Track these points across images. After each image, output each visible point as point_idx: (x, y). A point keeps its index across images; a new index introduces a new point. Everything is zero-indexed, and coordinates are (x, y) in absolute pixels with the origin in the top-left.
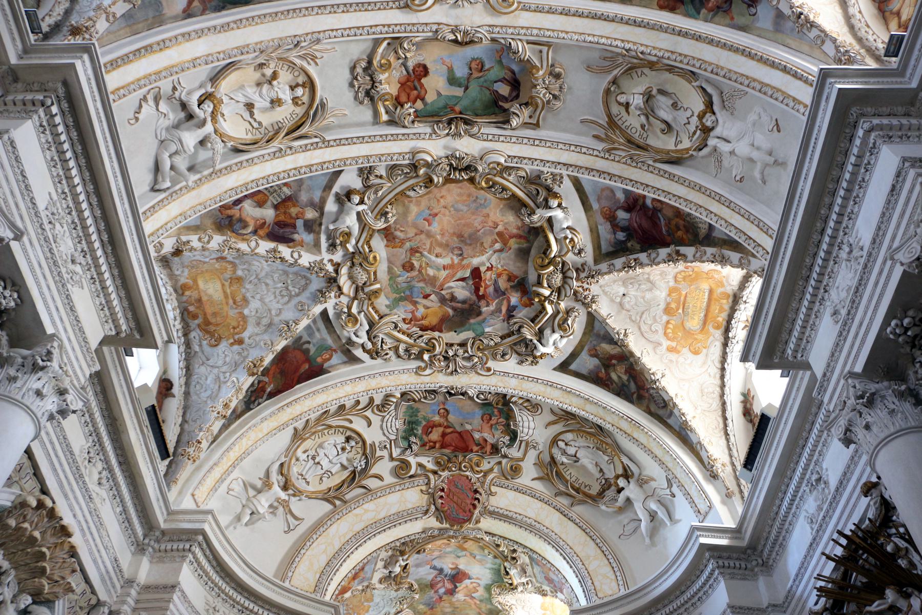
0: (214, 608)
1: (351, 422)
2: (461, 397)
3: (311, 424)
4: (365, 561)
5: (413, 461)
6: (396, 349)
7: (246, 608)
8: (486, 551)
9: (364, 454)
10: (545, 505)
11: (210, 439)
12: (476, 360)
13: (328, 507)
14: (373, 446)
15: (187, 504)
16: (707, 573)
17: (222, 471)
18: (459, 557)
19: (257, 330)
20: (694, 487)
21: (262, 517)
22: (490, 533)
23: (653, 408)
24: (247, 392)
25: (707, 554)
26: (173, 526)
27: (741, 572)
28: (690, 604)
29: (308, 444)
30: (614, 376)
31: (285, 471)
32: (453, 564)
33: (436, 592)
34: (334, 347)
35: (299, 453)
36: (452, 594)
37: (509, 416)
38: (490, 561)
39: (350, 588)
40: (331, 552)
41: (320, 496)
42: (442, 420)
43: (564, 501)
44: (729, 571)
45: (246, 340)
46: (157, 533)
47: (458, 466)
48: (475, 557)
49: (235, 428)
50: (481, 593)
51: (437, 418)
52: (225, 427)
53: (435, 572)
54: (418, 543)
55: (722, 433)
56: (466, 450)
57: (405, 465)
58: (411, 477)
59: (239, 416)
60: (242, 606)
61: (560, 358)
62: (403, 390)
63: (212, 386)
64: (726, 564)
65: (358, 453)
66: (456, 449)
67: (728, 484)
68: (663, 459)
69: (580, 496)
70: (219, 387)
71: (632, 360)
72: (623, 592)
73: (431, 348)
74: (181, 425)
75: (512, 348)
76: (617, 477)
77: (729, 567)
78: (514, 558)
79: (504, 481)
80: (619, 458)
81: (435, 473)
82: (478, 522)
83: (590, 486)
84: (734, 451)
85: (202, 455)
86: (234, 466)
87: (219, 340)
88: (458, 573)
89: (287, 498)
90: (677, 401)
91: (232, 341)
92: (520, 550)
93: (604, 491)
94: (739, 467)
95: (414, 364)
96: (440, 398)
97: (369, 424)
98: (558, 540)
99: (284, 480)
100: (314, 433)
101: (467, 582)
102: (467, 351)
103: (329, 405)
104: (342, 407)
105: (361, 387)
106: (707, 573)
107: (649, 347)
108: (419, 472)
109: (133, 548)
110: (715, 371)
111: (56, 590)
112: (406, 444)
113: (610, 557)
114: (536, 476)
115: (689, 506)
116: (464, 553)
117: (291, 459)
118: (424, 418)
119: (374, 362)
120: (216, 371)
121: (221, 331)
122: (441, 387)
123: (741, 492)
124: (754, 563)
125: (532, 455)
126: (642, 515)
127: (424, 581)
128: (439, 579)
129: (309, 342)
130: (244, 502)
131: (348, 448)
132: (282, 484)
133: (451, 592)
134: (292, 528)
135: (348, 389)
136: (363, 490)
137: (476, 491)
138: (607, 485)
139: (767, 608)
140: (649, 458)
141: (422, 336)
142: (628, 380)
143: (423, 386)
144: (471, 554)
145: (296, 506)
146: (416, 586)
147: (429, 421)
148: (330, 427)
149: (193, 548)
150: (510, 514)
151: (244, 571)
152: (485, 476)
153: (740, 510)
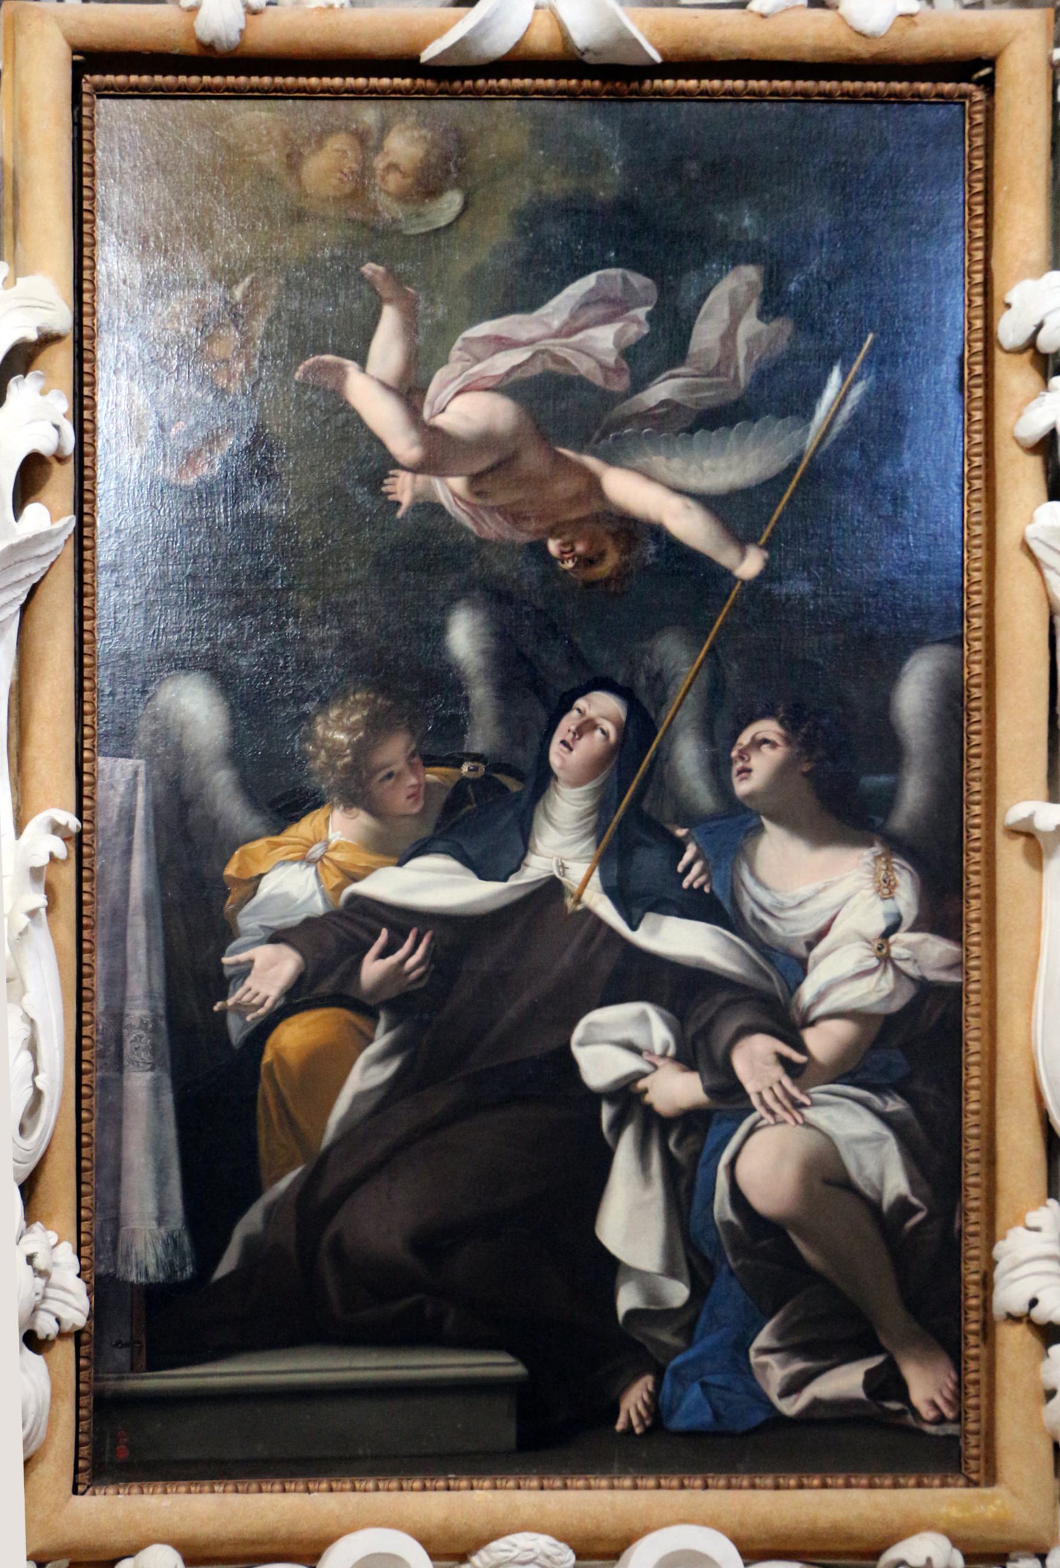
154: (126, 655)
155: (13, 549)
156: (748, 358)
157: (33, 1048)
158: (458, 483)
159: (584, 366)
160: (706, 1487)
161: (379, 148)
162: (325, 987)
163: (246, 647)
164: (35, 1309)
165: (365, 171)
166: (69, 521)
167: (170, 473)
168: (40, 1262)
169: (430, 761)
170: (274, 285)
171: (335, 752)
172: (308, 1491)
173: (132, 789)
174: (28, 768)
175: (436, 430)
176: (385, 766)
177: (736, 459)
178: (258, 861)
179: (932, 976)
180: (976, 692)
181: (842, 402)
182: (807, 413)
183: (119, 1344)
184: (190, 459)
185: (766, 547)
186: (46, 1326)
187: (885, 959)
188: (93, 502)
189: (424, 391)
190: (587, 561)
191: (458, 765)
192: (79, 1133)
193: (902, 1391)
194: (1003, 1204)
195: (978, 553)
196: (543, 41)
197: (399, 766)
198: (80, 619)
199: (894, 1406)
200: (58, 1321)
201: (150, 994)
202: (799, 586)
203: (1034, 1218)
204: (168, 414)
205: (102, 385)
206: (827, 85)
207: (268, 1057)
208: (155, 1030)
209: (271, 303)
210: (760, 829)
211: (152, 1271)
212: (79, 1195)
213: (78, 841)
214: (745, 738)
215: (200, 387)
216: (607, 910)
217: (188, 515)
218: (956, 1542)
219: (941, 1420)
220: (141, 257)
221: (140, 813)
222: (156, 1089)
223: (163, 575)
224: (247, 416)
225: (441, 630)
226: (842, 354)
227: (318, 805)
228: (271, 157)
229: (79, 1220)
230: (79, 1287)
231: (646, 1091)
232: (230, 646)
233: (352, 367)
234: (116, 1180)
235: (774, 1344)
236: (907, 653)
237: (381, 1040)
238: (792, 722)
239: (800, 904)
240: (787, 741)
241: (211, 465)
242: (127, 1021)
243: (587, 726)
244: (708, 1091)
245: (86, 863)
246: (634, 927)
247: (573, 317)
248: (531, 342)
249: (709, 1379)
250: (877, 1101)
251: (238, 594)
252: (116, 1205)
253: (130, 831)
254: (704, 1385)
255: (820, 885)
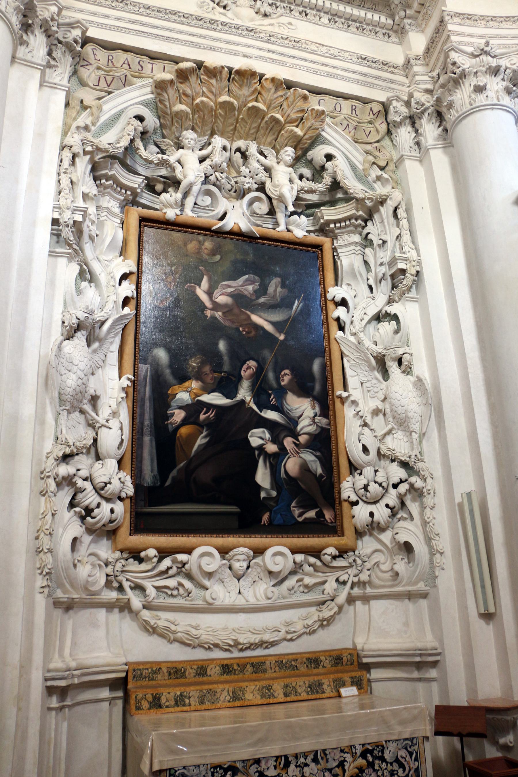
109: (394, 39)
111: (308, 124)
154: (146, 342)
155: (121, 316)
156: (279, 295)
157: (121, 429)
158: (220, 313)
159: (246, 293)
160: (282, 537)
161: (203, 245)
162: (192, 420)
163: (174, 343)
164: (121, 491)
165: (200, 248)
166: (134, 312)
167: (157, 304)
168: (122, 480)
169: (215, 372)
170: (181, 268)
171: (194, 368)
172: (188, 537)
173: (147, 371)
174: (123, 364)
175: (215, 302)
176: (205, 372)
177: (278, 315)
178: (176, 390)
179: (324, 426)
180: (328, 368)
181: (298, 306)
182: (292, 308)
183: (141, 500)
184: (162, 302)
185: (285, 334)
186: (123, 495)
187: (314, 422)
188: (140, 308)
189: (213, 294)
190: (248, 333)
191: (221, 373)
192: (132, 450)
193: (324, 516)
194: (341, 475)
195: (327, 339)
196: (236, 229)
197: (208, 372)
198: (136, 333)
199: (322, 519)
200: (126, 494)
201: (150, 419)
202: (292, 343)
203: (348, 479)
204: (157, 292)
205: (143, 284)
206: (291, 246)
207: (178, 435)
208: (151, 427)
209: (180, 272)
210: (287, 393)
211: (149, 483)
212: (132, 464)
213: (133, 382)
214: (283, 373)
215: (164, 287)
216: (255, 407)
217: (161, 313)
218: (337, 549)
219: (332, 522)
220: (152, 259)
221: (148, 377)
222: (151, 441)
223: (155, 326)
224: (175, 294)
225: (217, 344)
226: (298, 297)
227: (190, 379)
228: (181, 243)
229: (132, 470)
230: (131, 486)
231: (265, 448)
232: (170, 342)
233: (197, 287)
234: (141, 462)
235: (296, 505)
236: (314, 359)
237: (205, 433)
238: (292, 371)
239: (296, 409)
240: (291, 375)
241: (166, 303)
242: (144, 424)
243: (249, 368)
244: (278, 449)
245: (135, 387)
246: (261, 412)
247: (244, 283)
248: (235, 287)
249: (282, 513)
250: (314, 453)
251: (172, 331)
252: (141, 467)
253: (146, 381)
254: (281, 514)
255: (300, 405)
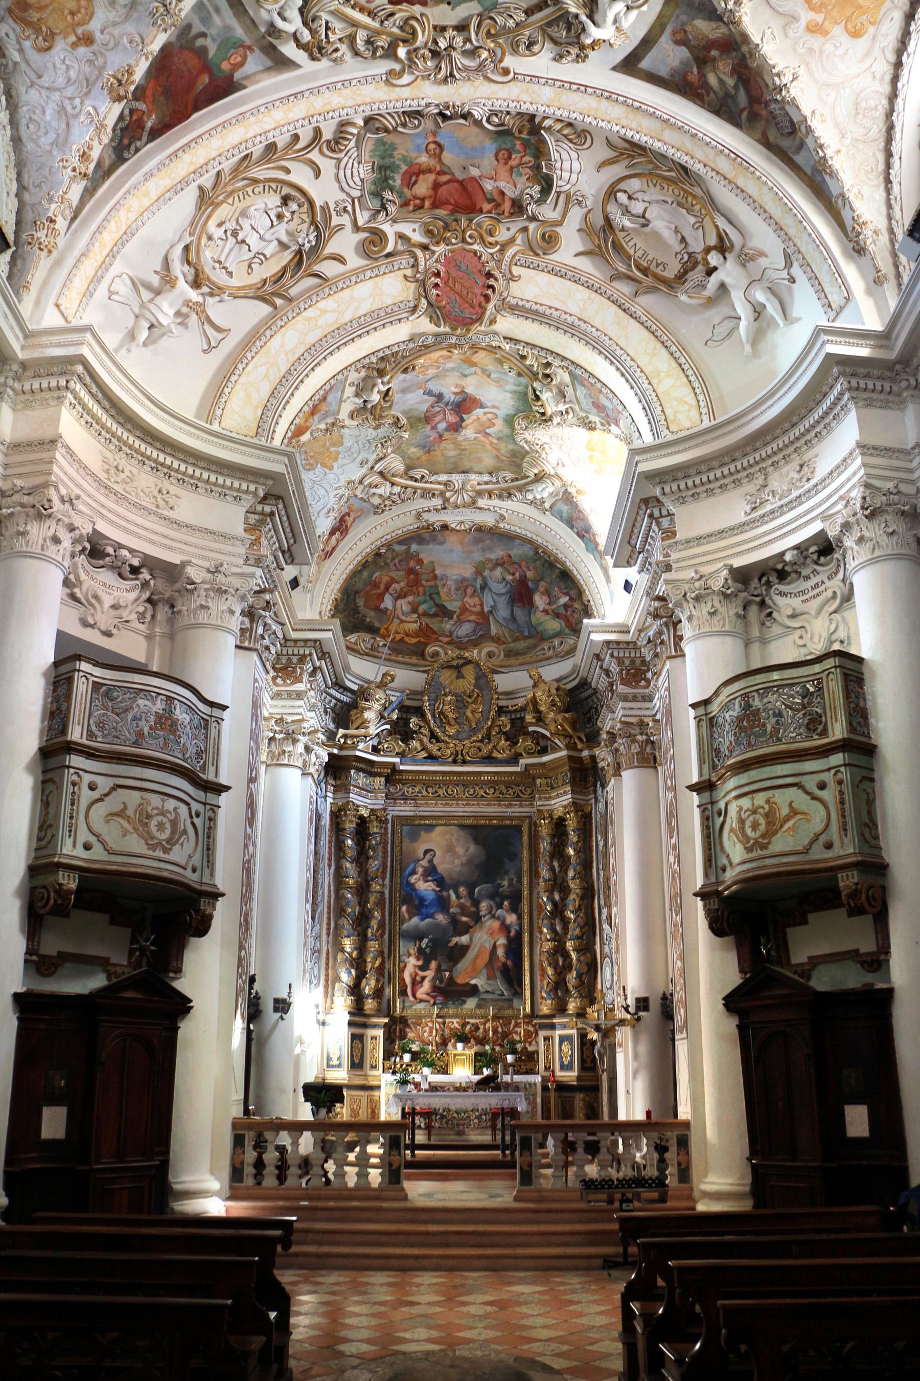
0: (116, 467)
1: (288, 171)
2: (462, 121)
3: (225, 178)
4: (328, 387)
5: (389, 230)
6: (352, 39)
7: (162, 465)
8: (506, 367)
9: (313, 222)
10: (594, 295)
11: (69, 214)
12: (485, 55)
13: (265, 309)
14: (325, 208)
15: (51, 319)
16: (832, 397)
17: (96, 265)
18: (466, 376)
19: (112, 16)
20: (826, 267)
21: (167, 332)
22: (511, 339)
23: (773, 136)
24: (114, 130)
25: (835, 370)
26: (36, 354)
27: (882, 397)
28: (802, 441)
29: (223, 212)
30: (712, 79)
31: (193, 257)
32: (457, 386)
33: (434, 428)
34: (248, 42)
35: (212, 226)
36: (456, 430)
37: (539, 151)
38: (511, 381)
39: (307, 428)
40: (275, 376)
41: (251, 293)
42: (432, 162)
43: (624, 288)
44: (866, 395)
45: (98, 35)
46: (15, 367)
47: (460, 236)
48: (489, 376)
49: (106, 193)
50: (499, 427)
51: (424, 159)
52: (88, 193)
53: (432, 399)
54: (404, 357)
55: (881, 179)
56: (472, 209)
57: (378, 236)
58: (389, 255)
59: (109, 173)
60: (155, 461)
61: (625, 48)
62: (368, 113)
63: (54, 124)
64: (862, 385)
65: (303, 222)
66: (457, 209)
67: (880, 263)
68: (781, 222)
69: (648, 281)
70: (68, 125)
71: (744, 49)
72: (706, 424)
73: (409, 37)
74: (17, 195)
75: (544, 32)
76: (708, 250)
77: (865, 390)
78: (547, 376)
79: (532, 258)
80: (712, 219)
81: (425, 248)
82: (493, 322)
83: (665, 265)
84: (897, 209)
85: (61, 242)
86: (112, 255)
87: (51, 37)
88: (464, 400)
89: (200, 299)
90: (813, 123)
91: (73, 38)
92: (556, 363)
93: (686, 272)
94: (900, 235)
95: (383, 66)
96: (428, 124)
97: (317, 173)
98: (614, 347)
99: (193, 271)
100: (232, 193)
101: (479, 412)
102: (468, 40)
103: (250, 144)
104: (271, 147)
105: (298, 110)
106: (832, 397)
107: (776, 24)
108: (400, 247)
110: (884, 68)
112: (377, 204)
113: (690, 372)
114: (582, 249)
115: (815, 297)
116: (473, 369)
117: (199, 239)
118: (405, 159)
119: (316, 65)
120: (56, 96)
121: (53, 21)
122: (428, 105)
123: (898, 276)
124: (904, 384)
125: (576, 215)
126: (742, 309)
127: (416, 414)
128: (437, 409)
129: (204, 35)
130: (137, 311)
131: (288, 214)
132: (190, 278)
133: (456, 428)
134: (213, 344)
135: (279, 115)
136: (316, 281)
137: (489, 275)
138: (690, 263)
139: (913, 448)
140: (759, 220)
141: (392, 14)
142: (736, 87)
143: (399, 105)
144: (484, 371)
145: (214, 309)
146: (404, 421)
147: (411, 165)
148: (255, 181)
149: (71, 384)
150: (541, 309)
151: (151, 411)
152: (502, 250)
153: (893, 304)
